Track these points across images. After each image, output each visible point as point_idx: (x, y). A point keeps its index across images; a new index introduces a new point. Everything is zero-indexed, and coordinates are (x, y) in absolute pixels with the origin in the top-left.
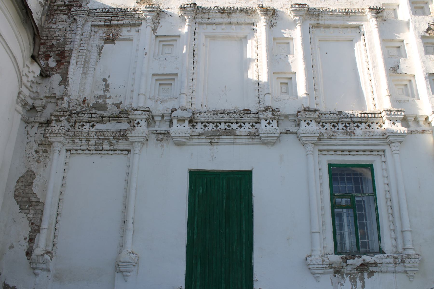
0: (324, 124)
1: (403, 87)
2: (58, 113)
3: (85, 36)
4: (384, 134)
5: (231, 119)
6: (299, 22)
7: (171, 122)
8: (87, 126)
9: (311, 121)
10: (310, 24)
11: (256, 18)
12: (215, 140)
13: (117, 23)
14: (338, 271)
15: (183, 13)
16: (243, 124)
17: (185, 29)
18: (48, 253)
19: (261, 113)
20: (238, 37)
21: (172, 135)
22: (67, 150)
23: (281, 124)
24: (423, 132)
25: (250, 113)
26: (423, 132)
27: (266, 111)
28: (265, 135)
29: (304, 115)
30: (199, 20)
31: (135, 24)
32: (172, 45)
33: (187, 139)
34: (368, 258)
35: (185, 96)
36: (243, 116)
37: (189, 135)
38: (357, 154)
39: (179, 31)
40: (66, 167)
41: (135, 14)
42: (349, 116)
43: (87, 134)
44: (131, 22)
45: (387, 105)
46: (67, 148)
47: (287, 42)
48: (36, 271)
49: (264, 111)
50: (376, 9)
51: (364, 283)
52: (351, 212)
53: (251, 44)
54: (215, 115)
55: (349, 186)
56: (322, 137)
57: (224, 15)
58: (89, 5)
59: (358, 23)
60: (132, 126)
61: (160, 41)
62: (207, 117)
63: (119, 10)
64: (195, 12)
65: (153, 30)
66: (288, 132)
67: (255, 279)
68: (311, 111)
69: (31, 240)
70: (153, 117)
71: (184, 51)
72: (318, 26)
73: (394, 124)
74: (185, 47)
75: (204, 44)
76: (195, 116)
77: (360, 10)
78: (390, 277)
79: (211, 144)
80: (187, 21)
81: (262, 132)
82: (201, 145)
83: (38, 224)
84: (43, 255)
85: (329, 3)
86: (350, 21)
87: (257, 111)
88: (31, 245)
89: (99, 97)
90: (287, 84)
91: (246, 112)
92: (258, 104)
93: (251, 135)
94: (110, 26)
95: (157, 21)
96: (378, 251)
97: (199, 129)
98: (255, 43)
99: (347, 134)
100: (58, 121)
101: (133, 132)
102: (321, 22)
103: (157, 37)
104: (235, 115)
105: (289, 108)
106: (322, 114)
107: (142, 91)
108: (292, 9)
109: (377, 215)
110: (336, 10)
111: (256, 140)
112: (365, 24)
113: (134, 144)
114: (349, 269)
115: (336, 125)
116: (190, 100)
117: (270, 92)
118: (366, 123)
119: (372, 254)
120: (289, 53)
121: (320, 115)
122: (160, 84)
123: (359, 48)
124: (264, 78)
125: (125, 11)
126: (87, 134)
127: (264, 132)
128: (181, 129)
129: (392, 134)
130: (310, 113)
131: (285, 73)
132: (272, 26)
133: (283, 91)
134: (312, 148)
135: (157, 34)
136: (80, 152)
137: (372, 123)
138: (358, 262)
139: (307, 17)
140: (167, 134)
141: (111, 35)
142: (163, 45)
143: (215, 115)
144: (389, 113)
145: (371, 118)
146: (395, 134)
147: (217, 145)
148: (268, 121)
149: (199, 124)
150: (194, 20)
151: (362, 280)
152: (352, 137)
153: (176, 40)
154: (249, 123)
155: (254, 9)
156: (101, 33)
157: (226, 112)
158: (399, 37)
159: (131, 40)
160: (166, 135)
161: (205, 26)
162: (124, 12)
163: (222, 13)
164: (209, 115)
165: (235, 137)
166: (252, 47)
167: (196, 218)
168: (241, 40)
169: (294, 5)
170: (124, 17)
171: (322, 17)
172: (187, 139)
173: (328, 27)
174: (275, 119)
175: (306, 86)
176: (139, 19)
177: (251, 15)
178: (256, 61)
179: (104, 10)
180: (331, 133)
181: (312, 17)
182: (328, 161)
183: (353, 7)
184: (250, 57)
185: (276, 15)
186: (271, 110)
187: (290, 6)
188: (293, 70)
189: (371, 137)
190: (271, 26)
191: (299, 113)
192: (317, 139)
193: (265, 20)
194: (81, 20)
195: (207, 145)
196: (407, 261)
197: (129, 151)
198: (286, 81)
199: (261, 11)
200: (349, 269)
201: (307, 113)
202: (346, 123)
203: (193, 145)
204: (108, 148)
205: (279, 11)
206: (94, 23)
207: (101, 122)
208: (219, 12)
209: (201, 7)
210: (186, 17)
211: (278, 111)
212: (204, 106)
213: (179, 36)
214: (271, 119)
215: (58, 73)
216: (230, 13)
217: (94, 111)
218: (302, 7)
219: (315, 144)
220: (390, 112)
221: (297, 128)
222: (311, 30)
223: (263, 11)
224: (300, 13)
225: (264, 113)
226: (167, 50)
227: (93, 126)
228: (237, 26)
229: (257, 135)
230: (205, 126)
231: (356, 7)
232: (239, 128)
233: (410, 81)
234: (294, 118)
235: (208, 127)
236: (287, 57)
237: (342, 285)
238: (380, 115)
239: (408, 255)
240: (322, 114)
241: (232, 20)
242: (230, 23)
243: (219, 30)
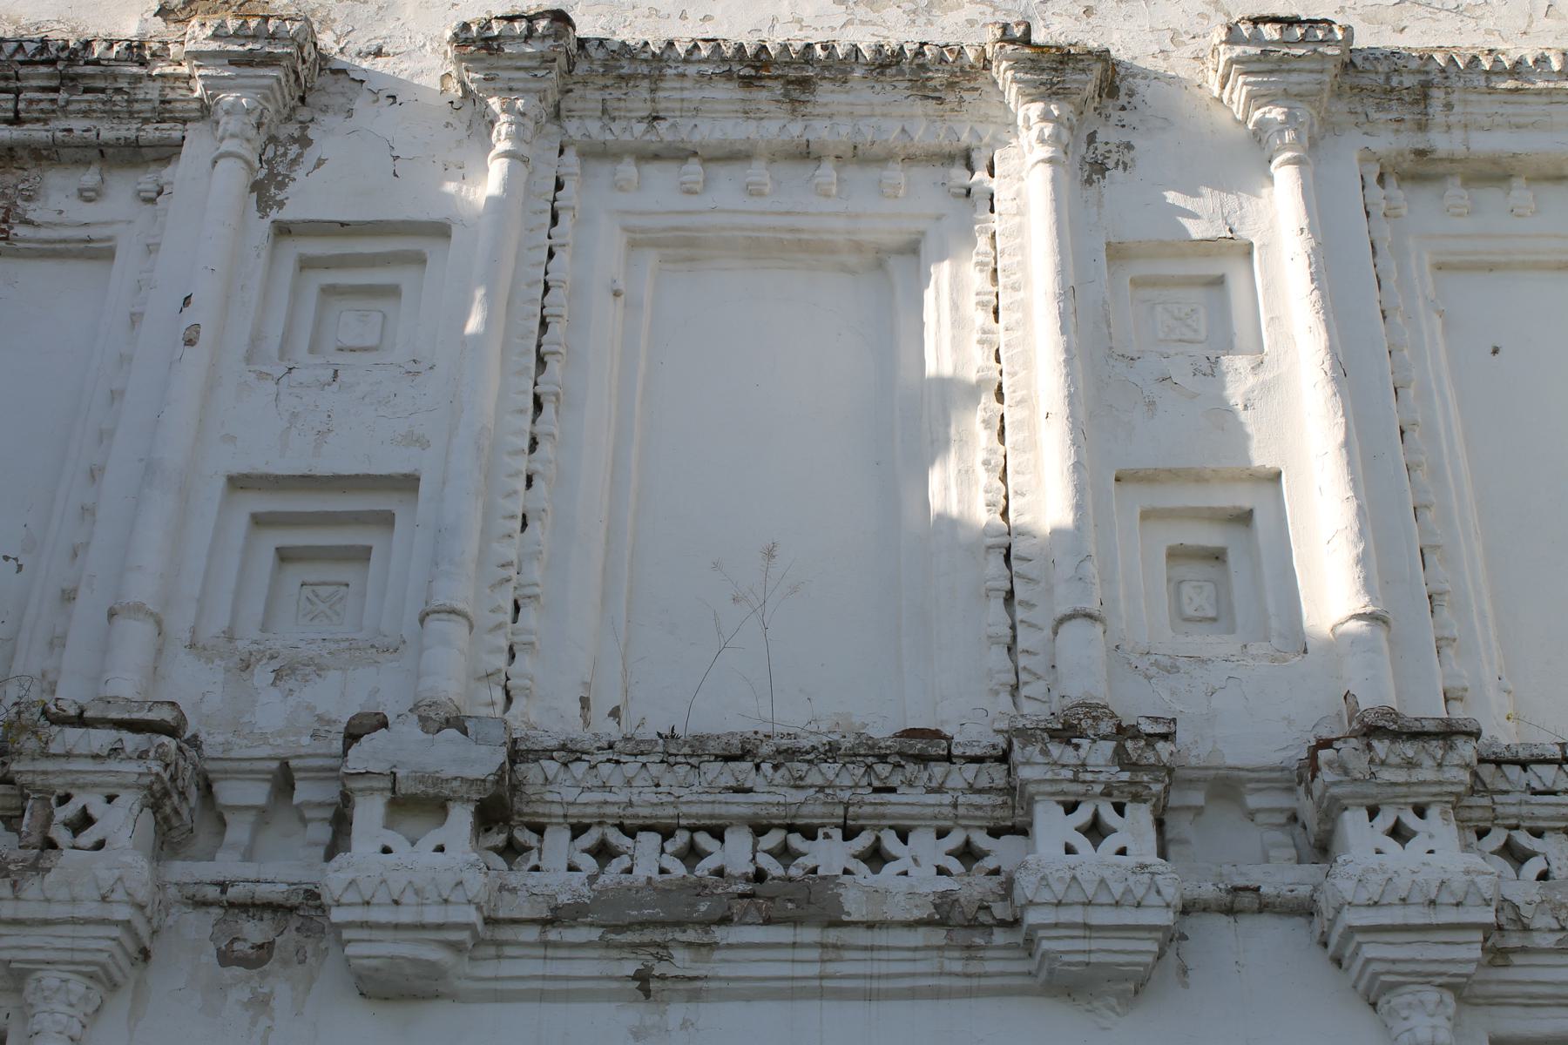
0: (1523, 839)
5: (799, 796)
6: (1289, 136)
7: (341, 822)
9: (1420, 811)
10: (1367, 156)
11: (986, 119)
12: (680, 955)
15: (474, 77)
16: (890, 842)
17: (490, 180)
19: (1033, 751)
20: (858, 247)
21: (337, 915)
23: (1183, 842)
25: (949, 758)
27: (1066, 733)
28: (1065, 915)
29: (1359, 765)
31: (135, 146)
32: (392, 291)
33: (456, 947)
35: (457, 629)
36: (895, 781)
37: (474, 916)
39: (449, 197)
41: (137, 79)
44: (108, 132)
47: (1212, 277)
49: (1054, 734)
54: (682, 770)
56: (1514, 941)
57: (764, 94)
60: (35, 838)
61: (306, 264)
62: (616, 780)
63: (30, 48)
64: (559, 74)
65: (257, 187)
66: (1246, 899)
68: (1415, 736)
70: (207, 788)
71: (474, 324)
72: (1420, 170)
74: (479, 293)
75: (621, 285)
76: (531, 772)
79: (647, 994)
80: (503, 127)
81: (1046, 896)
82: (568, 996)
85: (1488, 23)
87: (1001, 741)
90: (1217, 556)
91: (919, 745)
92: (1005, 699)
93: (956, 917)
95: (293, 129)
97: (558, 871)
98: (977, 280)
101: (32, 888)
102: (1442, 142)
103: (283, 230)
104: (830, 769)
105: (1243, 720)
106: (1499, 763)
107: (143, 589)
108: (1238, 50)
110: (1542, 60)
111: (998, 962)
113: (30, 985)
116: (501, 661)
117: (1094, 607)
120: (1229, 347)
121: (1487, 771)
122: (284, 556)
124: (1048, 503)
127: (1059, 889)
130: (1409, 749)
131: (1198, 477)
132: (1098, 168)
133: (1189, 611)
134: (1440, 1021)
135: (287, 214)
139: (1341, 107)
142: (329, 291)
143: (682, 770)
147: (695, 996)
148: (1083, 815)
150: (552, 128)
153: (419, 260)
154: (942, 834)
155: (971, 55)
157: (766, 749)
159: (96, 251)
160: (294, 922)
161: (628, 169)
162: (64, 66)
163: (747, 82)
164: (631, 768)
165: (833, 935)
166: (955, 307)
168: (880, 265)
169: (1246, 30)
170: (62, 96)
171: (1449, 106)
172: (456, 947)
173: (1495, 174)
174: (1136, 798)
175: (1362, 560)
176: (164, 112)
177: (951, 97)
178: (988, 399)
181: (1379, 107)
184: (947, 370)
185: (1123, 100)
186: (1106, 727)
187: (1221, 34)
188: (1261, 457)
190: (1089, 166)
191: (1324, 755)
192: (1476, 953)
193: (1048, 129)
195: (610, 996)
198: (1208, 536)
199: (1017, 63)
201: (1390, 752)
203: (500, 997)
208: (728, 76)
209: (601, 42)
210: (495, 103)
211: (1165, 737)
212: (599, 710)
213: (440, 230)
214: (1107, 793)
216: (804, 83)
218: (1303, 40)
219: (1461, 991)
221: (1311, 872)
222: (1375, 192)
223: (1033, 65)
224: (1294, 78)
225: (1056, 750)
226: (351, 323)
228: (853, 172)
229: (1002, 924)
230: (603, 852)
232: (862, 869)
234: (1285, 801)
235: (624, 862)
236: (1211, 371)
240: (1499, 763)
242: (806, 154)
243: (725, 198)
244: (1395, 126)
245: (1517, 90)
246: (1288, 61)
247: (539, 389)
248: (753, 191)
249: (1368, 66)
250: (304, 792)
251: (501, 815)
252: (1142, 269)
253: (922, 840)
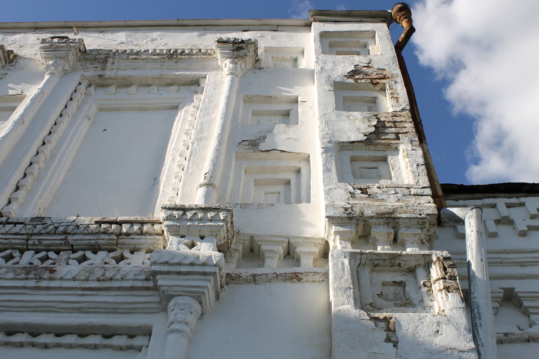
1: (280, 188)
10: (83, 77)
38: (59, 345)
42: (61, 229)
59: (193, 73)
72: (102, 83)
86: (177, 70)
99: (27, 273)
102: (108, 73)
115: (17, 254)
118: (110, 251)
123: (184, 121)
129: (166, 268)
137: (132, 252)
145: (127, 234)
152: (43, 284)
158: (291, 93)
171: (113, 63)
181: (91, 64)
220: (181, 213)
233: (299, 171)
244: (95, 69)
245: (136, 58)
246: (59, 48)
247: (26, 172)
249: (91, 53)
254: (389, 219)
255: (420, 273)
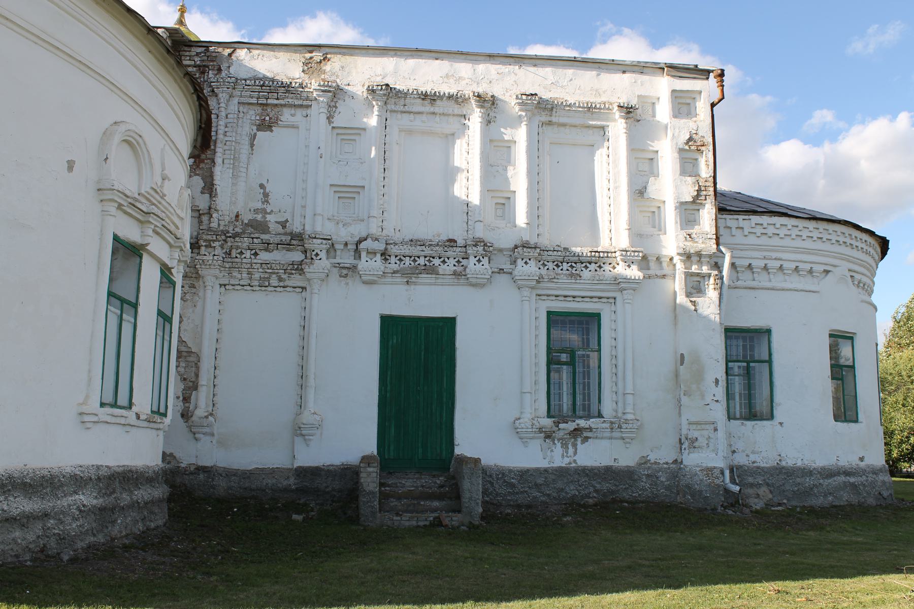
1: (650, 215)
2: (209, 237)
3: (231, 120)
4: (616, 279)
8: (248, 254)
13: (276, 102)
14: (548, 436)
17: (373, 121)
18: (211, 414)
22: (221, 285)
24: (664, 276)
26: (664, 276)
30: (391, 107)
34: (582, 423)
35: (375, 220)
40: (221, 307)
43: (249, 265)
44: (297, 102)
45: (623, 241)
46: (222, 283)
48: (197, 436)
50: (627, 108)
51: (576, 449)
52: (570, 369)
53: (460, 145)
55: (573, 338)
58: (232, 70)
65: (328, 118)
67: (456, 443)
69: (186, 399)
73: (629, 266)
74: (373, 148)
77: (607, 106)
78: (605, 443)
80: (376, 108)
83: (193, 380)
84: (206, 417)
86: (593, 120)
88: (187, 405)
89: (256, 211)
94: (267, 105)
95: (333, 104)
96: (596, 414)
97: (393, 265)
100: (208, 246)
101: (311, 267)
102: (554, 119)
103: (333, 128)
109: (600, 374)
112: (611, 124)
114: (561, 434)
117: (481, 219)
119: (588, 417)
123: (600, 156)
125: (288, 86)
126: (249, 265)
128: (370, 265)
132: (490, 122)
136: (239, 287)
138: (571, 426)
139: (536, 111)
140: (354, 268)
141: (267, 118)
144: (624, 253)
146: (628, 280)
149: (393, 258)
151: (575, 446)
156: (253, 114)
161: (399, 116)
162: (287, 88)
163: (423, 99)
167: (389, 373)
173: (564, 125)
176: (307, 99)
179: (257, 82)
180: (552, 274)
182: (548, 307)
183: (599, 100)
188: (512, 189)
189: (600, 281)
190: (488, 121)
194: (224, 95)
196: (624, 426)
197: (304, 288)
198: (503, 201)
199: (476, 101)
200: (561, 434)
201: (523, 248)
202: (572, 263)
204: (276, 285)
205: (500, 100)
206: (243, 100)
207: (267, 250)
210: (374, 103)
213: (364, 129)
215: (198, 175)
217: (257, 235)
222: (540, 129)
223: (479, 101)
227: (256, 254)
228: (442, 117)
231: (604, 99)
237: (552, 451)
238: (613, 255)
239: (626, 420)
241: (437, 110)
243: (418, 123)
248: (423, 122)
250: (349, 247)
251: (385, 255)
252: (496, 144)
253: (451, 259)
254: (699, 254)
255: (706, 278)
